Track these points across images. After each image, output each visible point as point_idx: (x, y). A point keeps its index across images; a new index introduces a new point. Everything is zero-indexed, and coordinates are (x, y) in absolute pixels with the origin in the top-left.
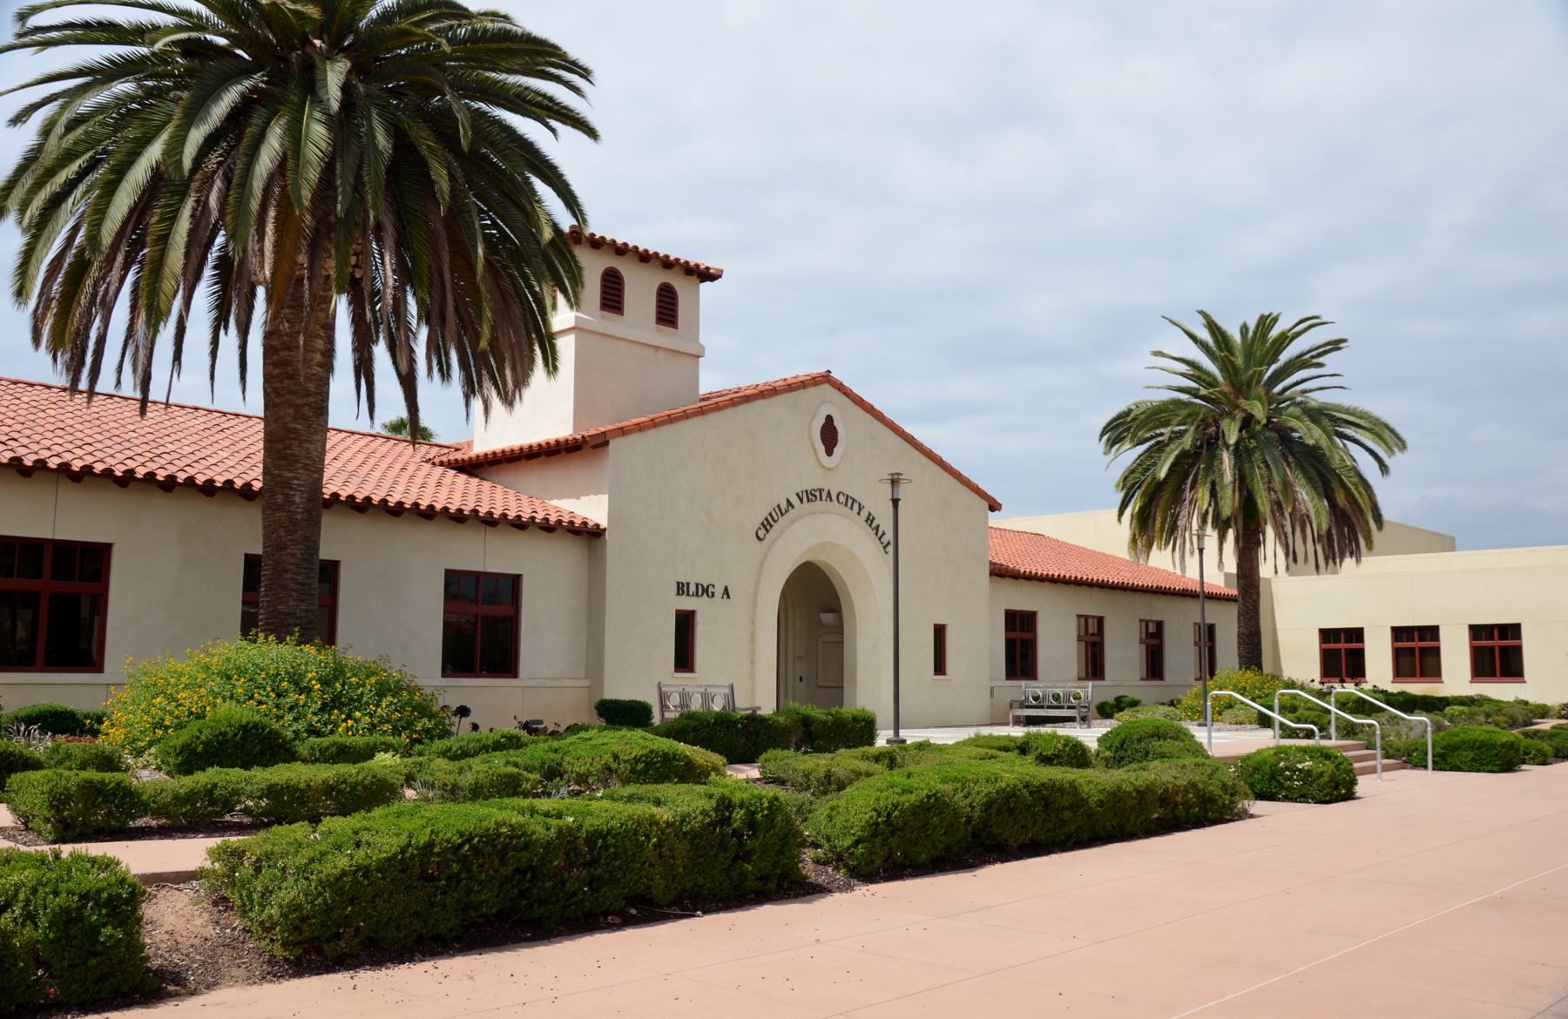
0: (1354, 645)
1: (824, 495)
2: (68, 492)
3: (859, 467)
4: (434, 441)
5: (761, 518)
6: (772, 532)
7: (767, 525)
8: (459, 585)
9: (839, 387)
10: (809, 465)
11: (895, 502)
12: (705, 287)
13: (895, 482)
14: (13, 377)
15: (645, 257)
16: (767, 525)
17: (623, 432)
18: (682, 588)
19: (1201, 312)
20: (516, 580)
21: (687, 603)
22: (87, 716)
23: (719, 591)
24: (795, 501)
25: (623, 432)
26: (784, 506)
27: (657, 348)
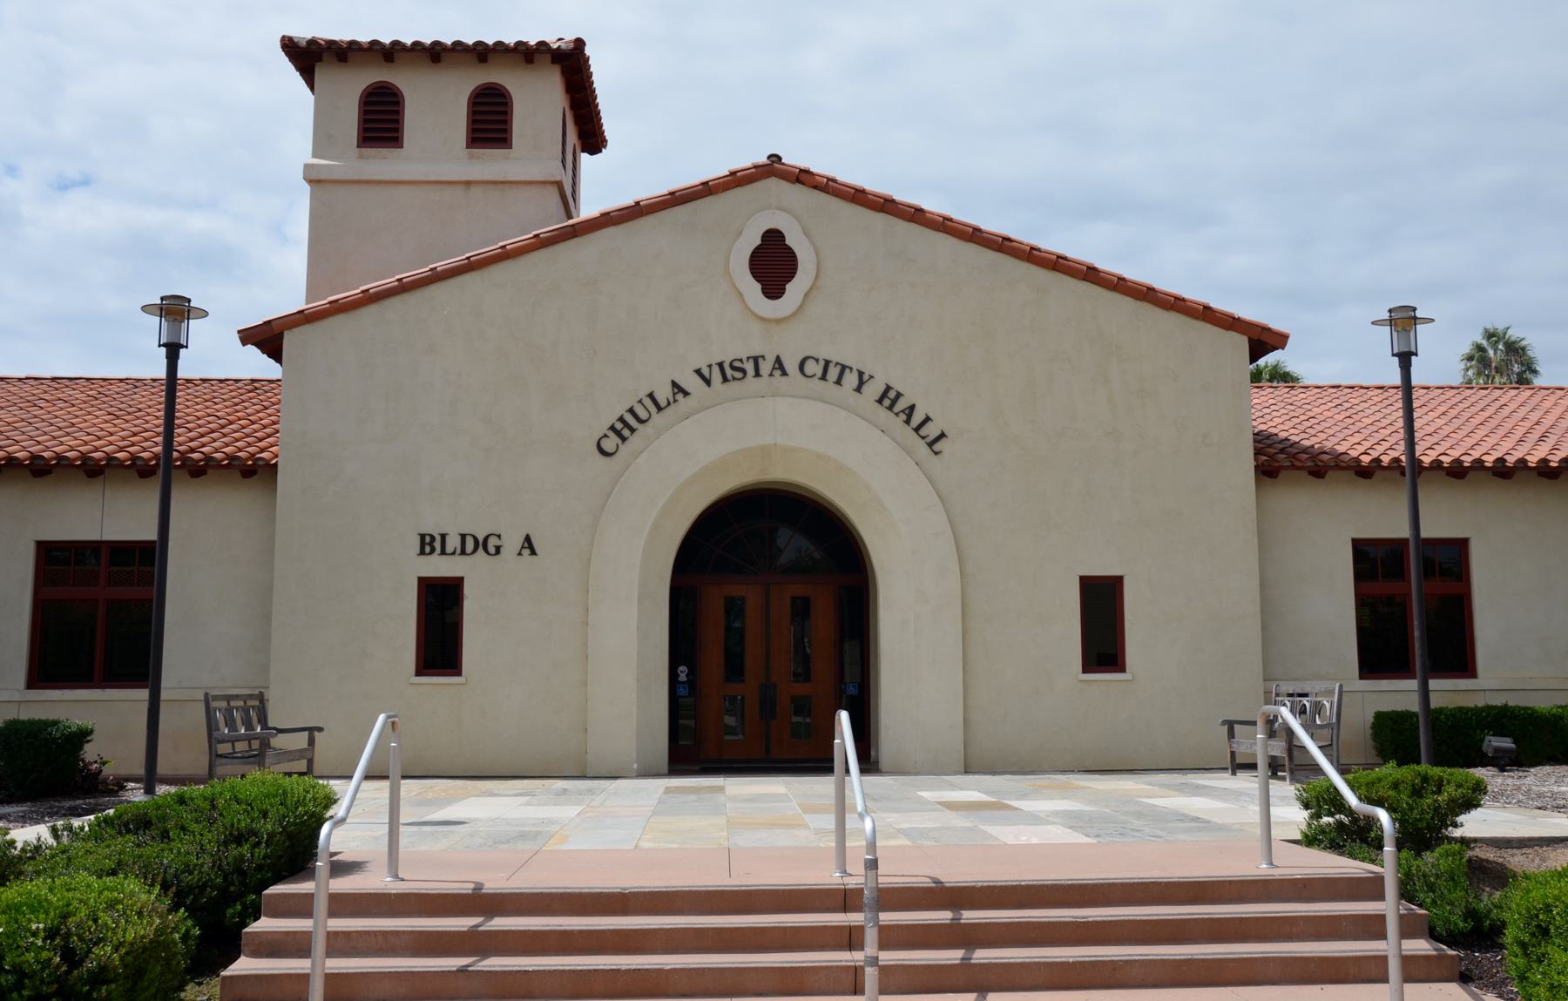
1: (765, 367)
3: (835, 304)
4: (1306, 382)
6: (635, 441)
7: (623, 429)
8: (1374, 562)
9: (803, 177)
10: (737, 315)
14: (222, 377)
15: (435, 54)
16: (623, 429)
23: (512, 543)
24: (691, 383)
26: (664, 394)
27: (468, 183)
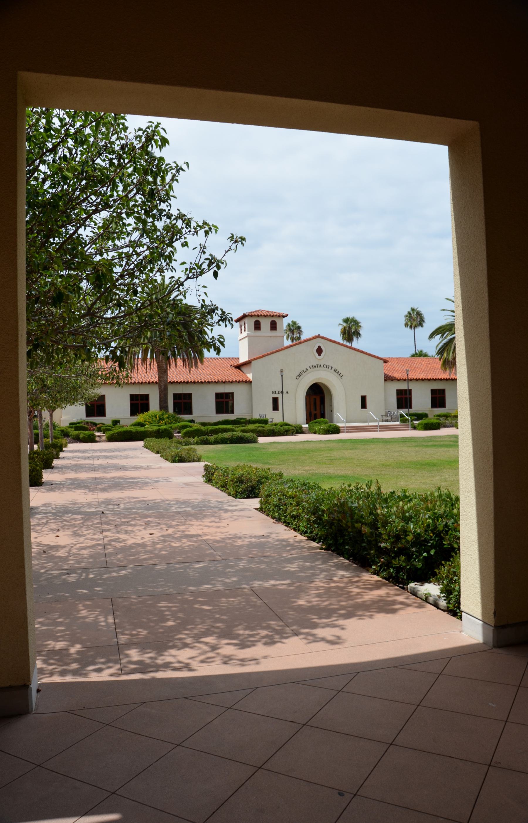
0: (134, 402)
2: (141, 386)
5: (298, 374)
6: (301, 377)
7: (299, 375)
8: (219, 396)
9: (323, 338)
10: (315, 359)
11: (282, 376)
12: (285, 319)
13: (282, 371)
16: (299, 375)
17: (255, 359)
18: (273, 392)
19: (288, 315)
20: (232, 394)
21: (275, 396)
22: (459, 505)
24: (309, 368)
25: (255, 359)
